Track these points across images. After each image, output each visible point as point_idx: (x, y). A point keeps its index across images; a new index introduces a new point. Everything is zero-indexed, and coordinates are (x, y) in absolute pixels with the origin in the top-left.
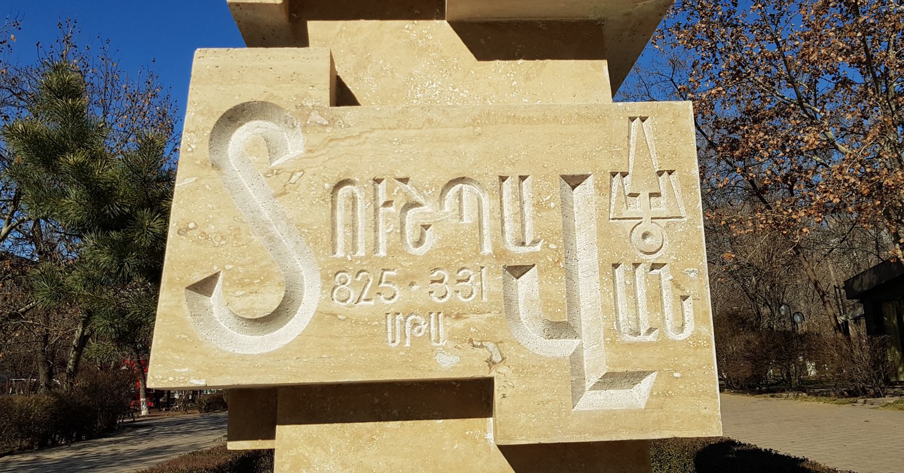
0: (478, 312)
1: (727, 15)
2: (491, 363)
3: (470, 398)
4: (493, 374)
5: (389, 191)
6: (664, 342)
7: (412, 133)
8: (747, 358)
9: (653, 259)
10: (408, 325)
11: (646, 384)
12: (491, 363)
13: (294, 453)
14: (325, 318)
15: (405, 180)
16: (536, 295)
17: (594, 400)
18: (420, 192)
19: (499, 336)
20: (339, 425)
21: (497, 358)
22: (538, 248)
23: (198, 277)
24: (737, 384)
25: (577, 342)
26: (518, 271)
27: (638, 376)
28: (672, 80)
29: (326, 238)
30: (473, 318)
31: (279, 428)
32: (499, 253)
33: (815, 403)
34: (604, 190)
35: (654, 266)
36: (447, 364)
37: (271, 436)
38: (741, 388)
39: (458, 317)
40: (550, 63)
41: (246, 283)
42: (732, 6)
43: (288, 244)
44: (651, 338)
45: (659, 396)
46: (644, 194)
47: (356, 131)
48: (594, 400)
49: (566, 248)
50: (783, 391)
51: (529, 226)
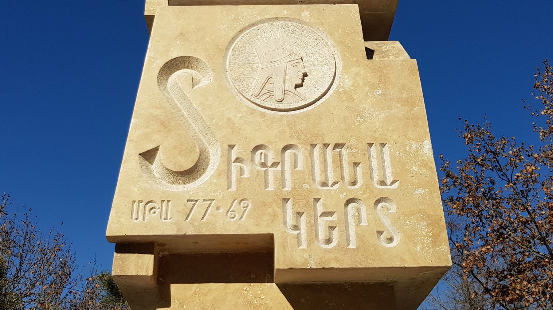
1: (487, 191)
42: (491, 185)
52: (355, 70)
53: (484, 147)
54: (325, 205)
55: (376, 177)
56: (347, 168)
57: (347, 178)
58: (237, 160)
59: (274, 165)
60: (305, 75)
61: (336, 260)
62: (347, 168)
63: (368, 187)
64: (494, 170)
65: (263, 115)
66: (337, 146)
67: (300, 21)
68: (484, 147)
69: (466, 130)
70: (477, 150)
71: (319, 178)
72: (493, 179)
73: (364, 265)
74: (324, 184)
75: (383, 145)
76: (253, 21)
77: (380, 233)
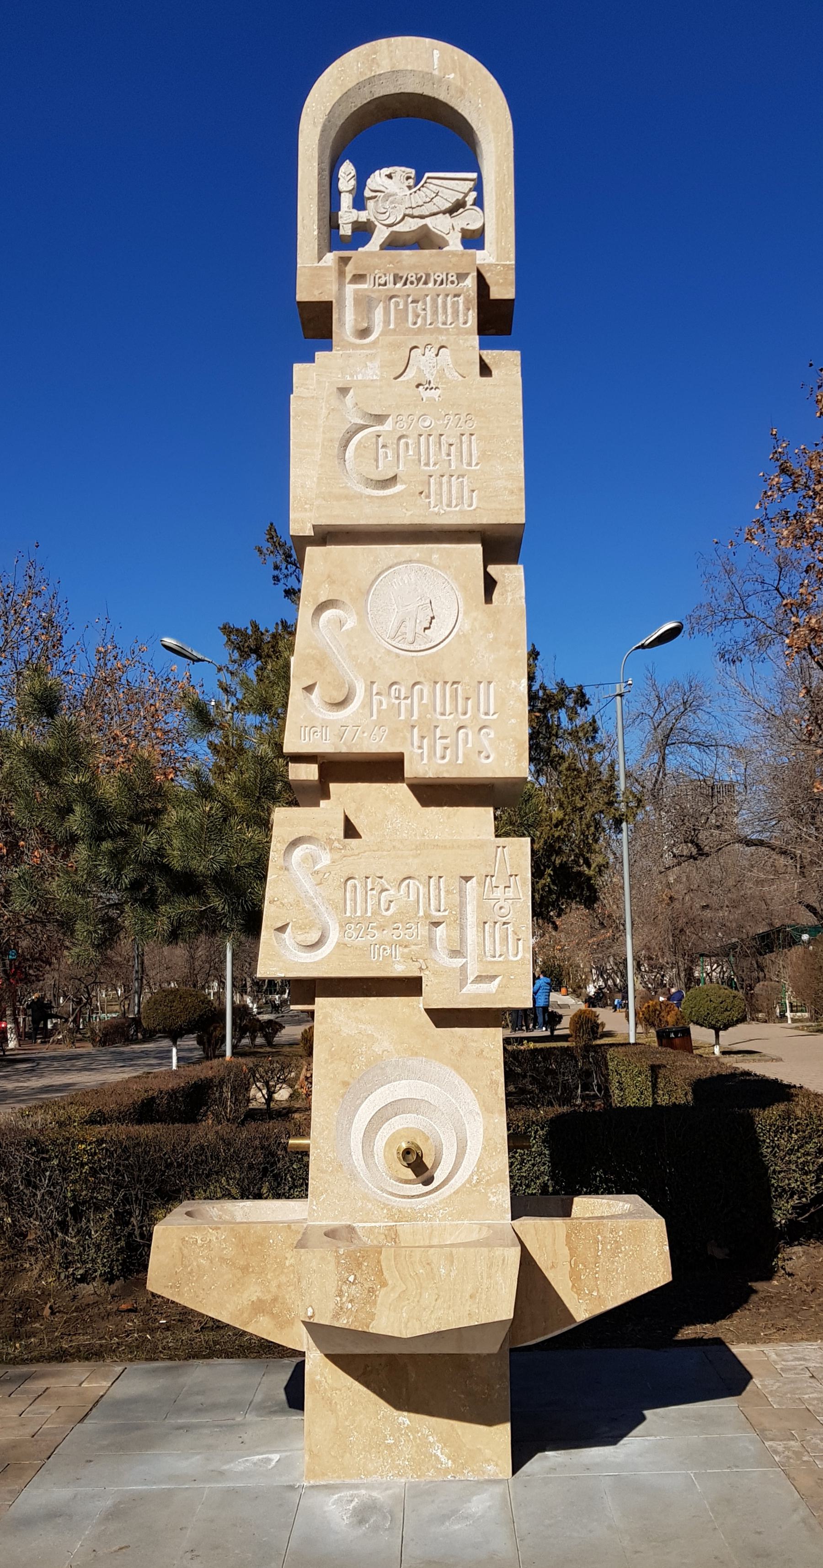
0: (415, 944)
2: (421, 969)
3: (410, 986)
4: (422, 975)
5: (373, 883)
6: (507, 961)
7: (385, 853)
9: (504, 920)
10: (381, 950)
12: (421, 969)
13: (324, 1011)
15: (381, 878)
17: (471, 988)
18: (388, 884)
21: (424, 967)
22: (446, 913)
23: (280, 925)
25: (465, 960)
26: (437, 924)
27: (494, 977)
28: (777, 589)
29: (341, 906)
30: (413, 947)
31: (316, 999)
32: (427, 915)
35: (504, 923)
36: (400, 969)
37: (313, 1003)
39: (406, 947)
40: (461, 809)
41: (303, 928)
46: (502, 887)
47: (356, 852)
49: (461, 914)
58: (383, 446)
60: (437, 355)
61: (447, 771)
67: (431, 564)
76: (391, 563)
77: (480, 752)
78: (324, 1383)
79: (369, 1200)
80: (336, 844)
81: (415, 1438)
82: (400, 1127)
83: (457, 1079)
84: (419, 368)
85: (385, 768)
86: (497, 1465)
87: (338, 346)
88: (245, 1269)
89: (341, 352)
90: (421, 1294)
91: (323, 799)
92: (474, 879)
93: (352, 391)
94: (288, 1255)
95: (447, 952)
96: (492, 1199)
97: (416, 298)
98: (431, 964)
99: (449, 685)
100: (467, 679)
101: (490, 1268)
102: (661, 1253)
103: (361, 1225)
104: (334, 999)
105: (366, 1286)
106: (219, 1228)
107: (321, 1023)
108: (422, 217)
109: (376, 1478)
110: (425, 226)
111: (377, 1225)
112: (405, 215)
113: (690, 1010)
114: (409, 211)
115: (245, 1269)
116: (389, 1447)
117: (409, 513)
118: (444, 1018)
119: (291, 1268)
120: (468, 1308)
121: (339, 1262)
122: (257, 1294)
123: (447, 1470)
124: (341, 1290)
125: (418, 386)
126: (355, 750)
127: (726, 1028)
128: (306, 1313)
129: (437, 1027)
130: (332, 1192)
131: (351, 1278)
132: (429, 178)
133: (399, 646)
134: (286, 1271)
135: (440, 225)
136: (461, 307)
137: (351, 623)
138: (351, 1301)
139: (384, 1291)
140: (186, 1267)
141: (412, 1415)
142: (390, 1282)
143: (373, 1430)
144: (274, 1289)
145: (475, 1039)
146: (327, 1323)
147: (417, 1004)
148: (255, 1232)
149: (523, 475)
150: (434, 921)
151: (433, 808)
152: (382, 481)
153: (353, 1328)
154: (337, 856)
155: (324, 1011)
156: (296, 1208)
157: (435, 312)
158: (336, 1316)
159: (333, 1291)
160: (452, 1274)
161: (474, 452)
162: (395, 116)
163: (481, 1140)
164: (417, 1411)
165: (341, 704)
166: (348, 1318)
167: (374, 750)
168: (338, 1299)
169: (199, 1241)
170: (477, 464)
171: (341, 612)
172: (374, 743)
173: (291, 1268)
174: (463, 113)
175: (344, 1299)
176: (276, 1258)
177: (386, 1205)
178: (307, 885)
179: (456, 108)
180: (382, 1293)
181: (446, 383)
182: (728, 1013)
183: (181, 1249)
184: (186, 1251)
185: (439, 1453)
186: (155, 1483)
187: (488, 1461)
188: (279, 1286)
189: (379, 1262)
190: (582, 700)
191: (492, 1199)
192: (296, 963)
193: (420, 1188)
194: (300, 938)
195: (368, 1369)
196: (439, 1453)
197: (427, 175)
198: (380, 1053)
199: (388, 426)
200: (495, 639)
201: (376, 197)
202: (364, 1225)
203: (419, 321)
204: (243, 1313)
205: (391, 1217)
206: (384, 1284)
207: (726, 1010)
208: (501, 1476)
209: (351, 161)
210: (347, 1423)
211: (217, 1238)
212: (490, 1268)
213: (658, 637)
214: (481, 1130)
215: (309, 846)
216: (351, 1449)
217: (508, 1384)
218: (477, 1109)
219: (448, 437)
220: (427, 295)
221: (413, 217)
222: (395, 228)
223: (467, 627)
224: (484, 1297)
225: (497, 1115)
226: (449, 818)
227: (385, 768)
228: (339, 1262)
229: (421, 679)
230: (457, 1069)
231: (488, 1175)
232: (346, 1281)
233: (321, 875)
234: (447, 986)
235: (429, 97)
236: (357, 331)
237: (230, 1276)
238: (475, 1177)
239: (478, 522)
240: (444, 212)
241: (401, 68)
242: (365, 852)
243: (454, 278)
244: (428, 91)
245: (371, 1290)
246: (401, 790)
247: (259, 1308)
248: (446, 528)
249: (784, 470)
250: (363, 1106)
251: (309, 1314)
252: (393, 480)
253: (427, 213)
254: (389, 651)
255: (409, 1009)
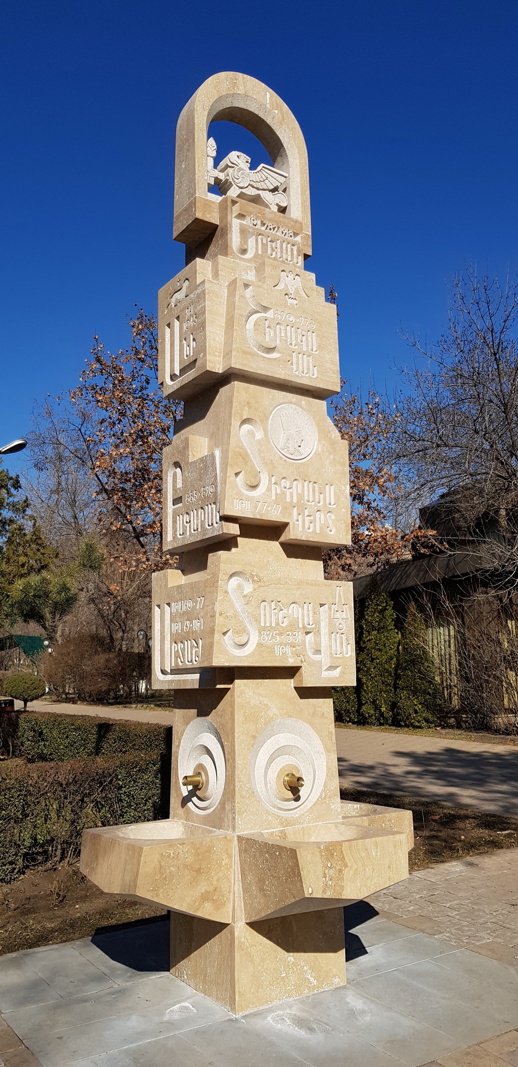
0: (299, 646)
1: (139, 389)
3: (290, 672)
5: (276, 605)
6: (344, 657)
7: (282, 586)
8: (106, 675)
9: (341, 631)
10: (281, 649)
11: (338, 670)
12: (302, 661)
13: (240, 688)
14: (260, 645)
15: (279, 602)
16: (313, 641)
17: (325, 674)
18: (283, 606)
19: (304, 653)
20: (252, 680)
21: (303, 660)
22: (313, 626)
24: (90, 697)
26: (307, 633)
27: (337, 667)
28: (80, 430)
32: (304, 627)
33: (163, 712)
34: (330, 609)
35: (342, 634)
36: (291, 662)
38: (93, 701)
39: (294, 647)
41: (237, 633)
42: (145, 383)
43: (246, 621)
44: (340, 656)
45: (342, 673)
46: (340, 611)
48: (325, 674)
50: (131, 703)
51: (311, 619)
52: (323, 442)
53: (150, 341)
54: (309, 512)
55: (328, 502)
56: (317, 494)
57: (317, 500)
59: (290, 488)
61: (312, 537)
62: (317, 494)
63: (325, 504)
64: (153, 369)
65: (286, 461)
66: (315, 483)
68: (150, 341)
69: (138, 319)
70: (142, 344)
71: (306, 498)
72: (149, 378)
73: (322, 541)
74: (308, 501)
75: (331, 485)
77: (328, 527)
78: (246, 943)
79: (270, 815)
80: (255, 578)
81: (297, 969)
82: (284, 764)
83: (311, 732)
84: (285, 284)
85: (269, 530)
86: (339, 978)
87: (231, 255)
88: (198, 871)
89: (233, 260)
90: (365, 869)
91: (235, 547)
92: (326, 605)
93: (251, 287)
94: (224, 858)
95: (313, 650)
96: (333, 807)
97: (273, 239)
98: (307, 658)
99: (311, 483)
100: (320, 481)
101: (395, 848)
102: (410, 831)
103: (266, 831)
104: (246, 680)
105: (337, 868)
106: (184, 843)
107: (239, 697)
108: (258, 189)
109: (276, 1002)
110: (259, 195)
111: (274, 830)
112: (249, 185)
113: (11, 688)
114: (251, 183)
115: (198, 871)
116: (283, 978)
117: (283, 372)
118: (305, 693)
119: (226, 866)
120: (388, 875)
121: (322, 855)
122: (205, 888)
123: (314, 987)
124: (325, 873)
125: (286, 294)
126: (265, 518)
127: (32, 700)
128: (308, 892)
129: (301, 698)
130: (249, 811)
131: (329, 865)
132: (263, 167)
133: (285, 454)
134: (222, 868)
135: (267, 196)
136: (295, 252)
137: (259, 436)
138: (331, 880)
139: (347, 869)
140: (163, 874)
141: (295, 954)
142: (349, 864)
143: (274, 969)
144: (215, 883)
145: (320, 705)
146: (320, 897)
147: (291, 683)
148: (206, 844)
149: (338, 363)
150: (308, 631)
151: (293, 559)
152: (268, 349)
153: (333, 897)
154: (256, 586)
155: (240, 688)
156: (166, 826)
157: (282, 252)
158: (324, 891)
159: (320, 874)
160: (378, 854)
161: (315, 343)
162: (231, 120)
163: (325, 769)
164: (297, 951)
165: (254, 487)
166: (330, 891)
167: (274, 519)
168: (324, 879)
169: (172, 855)
170: (316, 351)
171: (252, 427)
172: (274, 515)
173: (226, 866)
174: (279, 135)
175: (327, 879)
176: (217, 860)
177: (278, 816)
178: (239, 605)
179: (276, 131)
180: (345, 872)
181: (300, 298)
182: (36, 691)
183: (160, 861)
184: (163, 863)
185: (309, 977)
186: (132, 1043)
187: (334, 976)
188: (218, 880)
189: (342, 852)
190: (17, 485)
191: (333, 807)
192: (235, 656)
193: (294, 804)
194: (237, 640)
195: (271, 928)
196: (309, 977)
197: (262, 165)
198: (272, 716)
199: (270, 314)
200: (334, 459)
201: (233, 167)
202: (268, 831)
203: (274, 253)
204: (196, 902)
205: (282, 824)
206: (346, 866)
207: (35, 689)
208: (341, 984)
209: (215, 140)
210: (260, 968)
211: (183, 851)
212: (395, 848)
213: (11, 448)
214: (325, 764)
215: (239, 578)
216: (262, 985)
217: (343, 924)
218: (322, 749)
219: (302, 330)
220: (278, 240)
221: (253, 187)
222: (244, 190)
223: (320, 450)
224: (395, 866)
225: (332, 754)
226: (301, 566)
227: (269, 530)
228: (322, 855)
229: (298, 478)
230: (311, 724)
231: (330, 792)
232: (326, 867)
233: (248, 598)
234: (315, 672)
235: (260, 118)
236: (241, 249)
237: (189, 877)
238: (324, 794)
239: (318, 386)
240: (270, 191)
241: (250, 95)
242: (271, 584)
243: (292, 234)
244: (261, 115)
245: (340, 871)
246: (275, 546)
247: (206, 897)
248: (299, 386)
249: (98, 360)
250: (261, 751)
251: (310, 892)
252: (271, 350)
253: (261, 188)
254: (281, 458)
255: (287, 686)
